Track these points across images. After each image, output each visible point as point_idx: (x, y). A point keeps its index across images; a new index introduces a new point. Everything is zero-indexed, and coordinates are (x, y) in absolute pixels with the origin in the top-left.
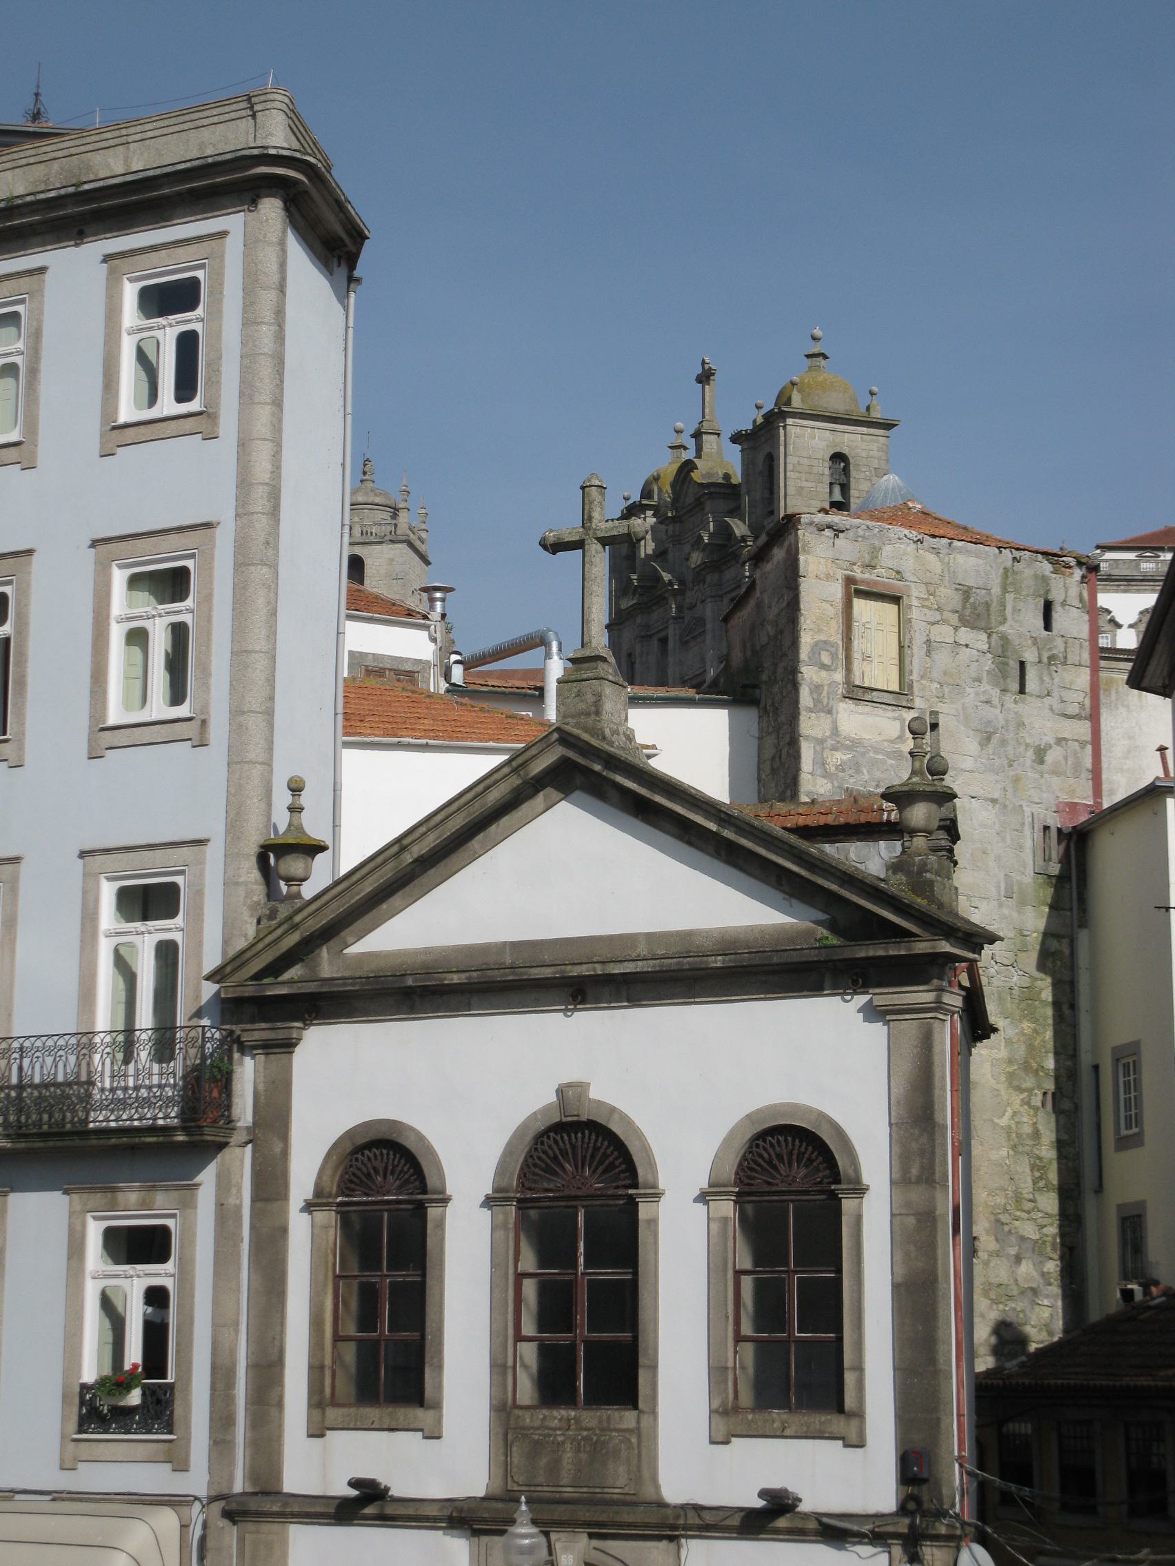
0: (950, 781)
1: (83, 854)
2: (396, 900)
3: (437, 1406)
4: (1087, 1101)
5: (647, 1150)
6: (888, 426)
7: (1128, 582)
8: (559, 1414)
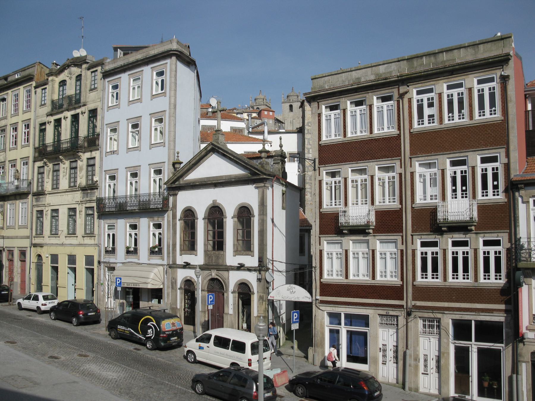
2: (191, 171)
3: (197, 251)
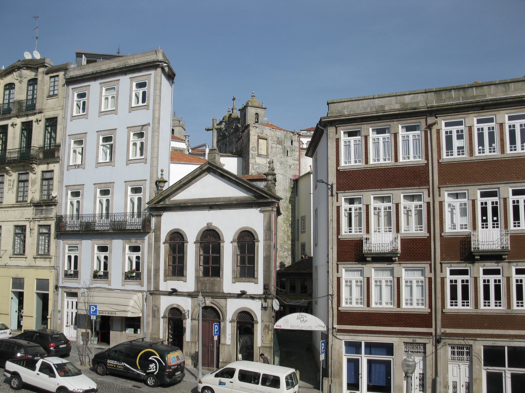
0: (275, 172)
1: (125, 182)
2: (179, 191)
3: (186, 277)
4: (297, 226)
5: (222, 234)
6: (265, 109)
7: (305, 136)
8: (206, 278)
